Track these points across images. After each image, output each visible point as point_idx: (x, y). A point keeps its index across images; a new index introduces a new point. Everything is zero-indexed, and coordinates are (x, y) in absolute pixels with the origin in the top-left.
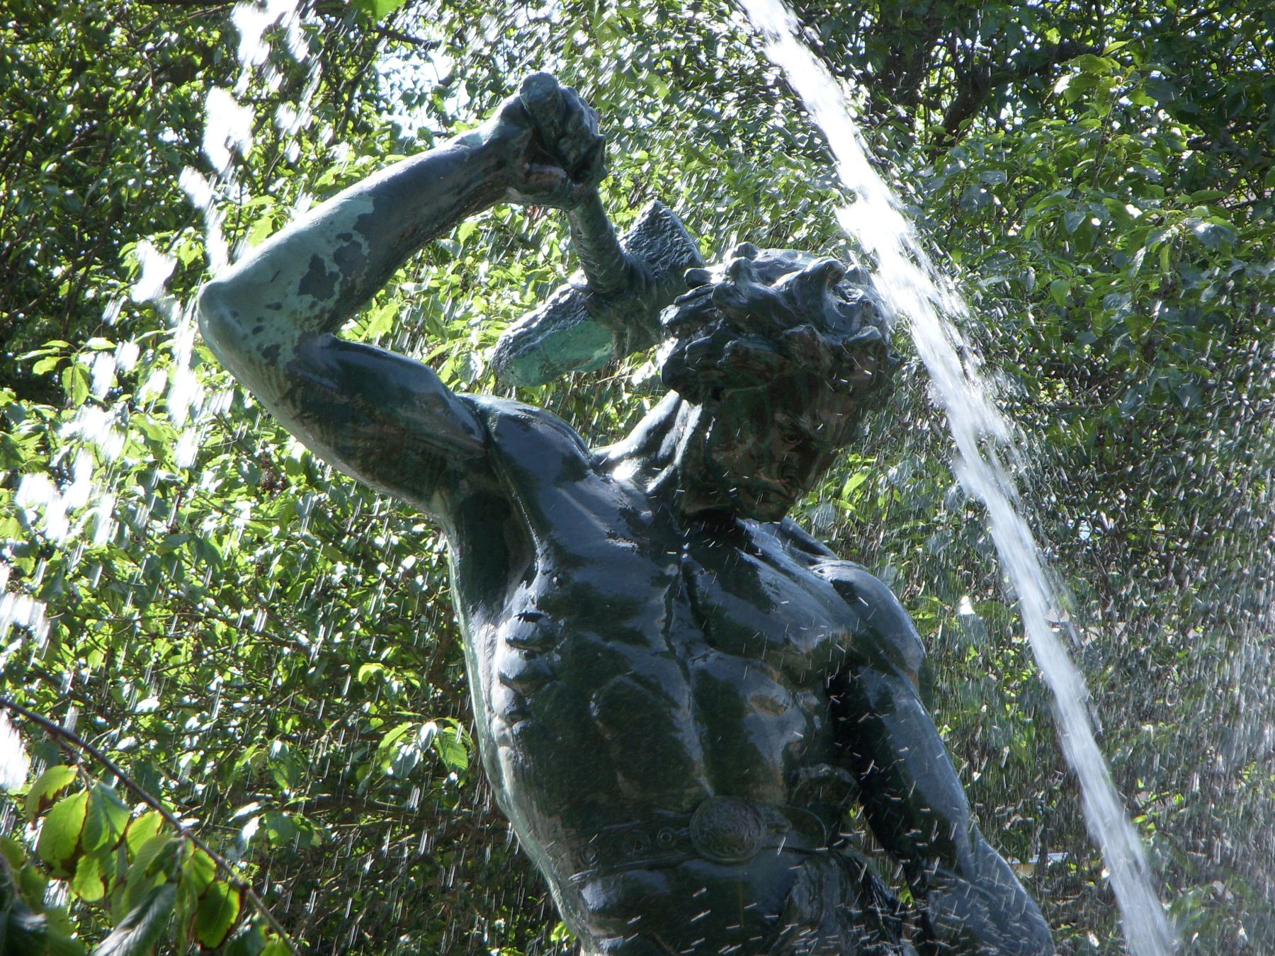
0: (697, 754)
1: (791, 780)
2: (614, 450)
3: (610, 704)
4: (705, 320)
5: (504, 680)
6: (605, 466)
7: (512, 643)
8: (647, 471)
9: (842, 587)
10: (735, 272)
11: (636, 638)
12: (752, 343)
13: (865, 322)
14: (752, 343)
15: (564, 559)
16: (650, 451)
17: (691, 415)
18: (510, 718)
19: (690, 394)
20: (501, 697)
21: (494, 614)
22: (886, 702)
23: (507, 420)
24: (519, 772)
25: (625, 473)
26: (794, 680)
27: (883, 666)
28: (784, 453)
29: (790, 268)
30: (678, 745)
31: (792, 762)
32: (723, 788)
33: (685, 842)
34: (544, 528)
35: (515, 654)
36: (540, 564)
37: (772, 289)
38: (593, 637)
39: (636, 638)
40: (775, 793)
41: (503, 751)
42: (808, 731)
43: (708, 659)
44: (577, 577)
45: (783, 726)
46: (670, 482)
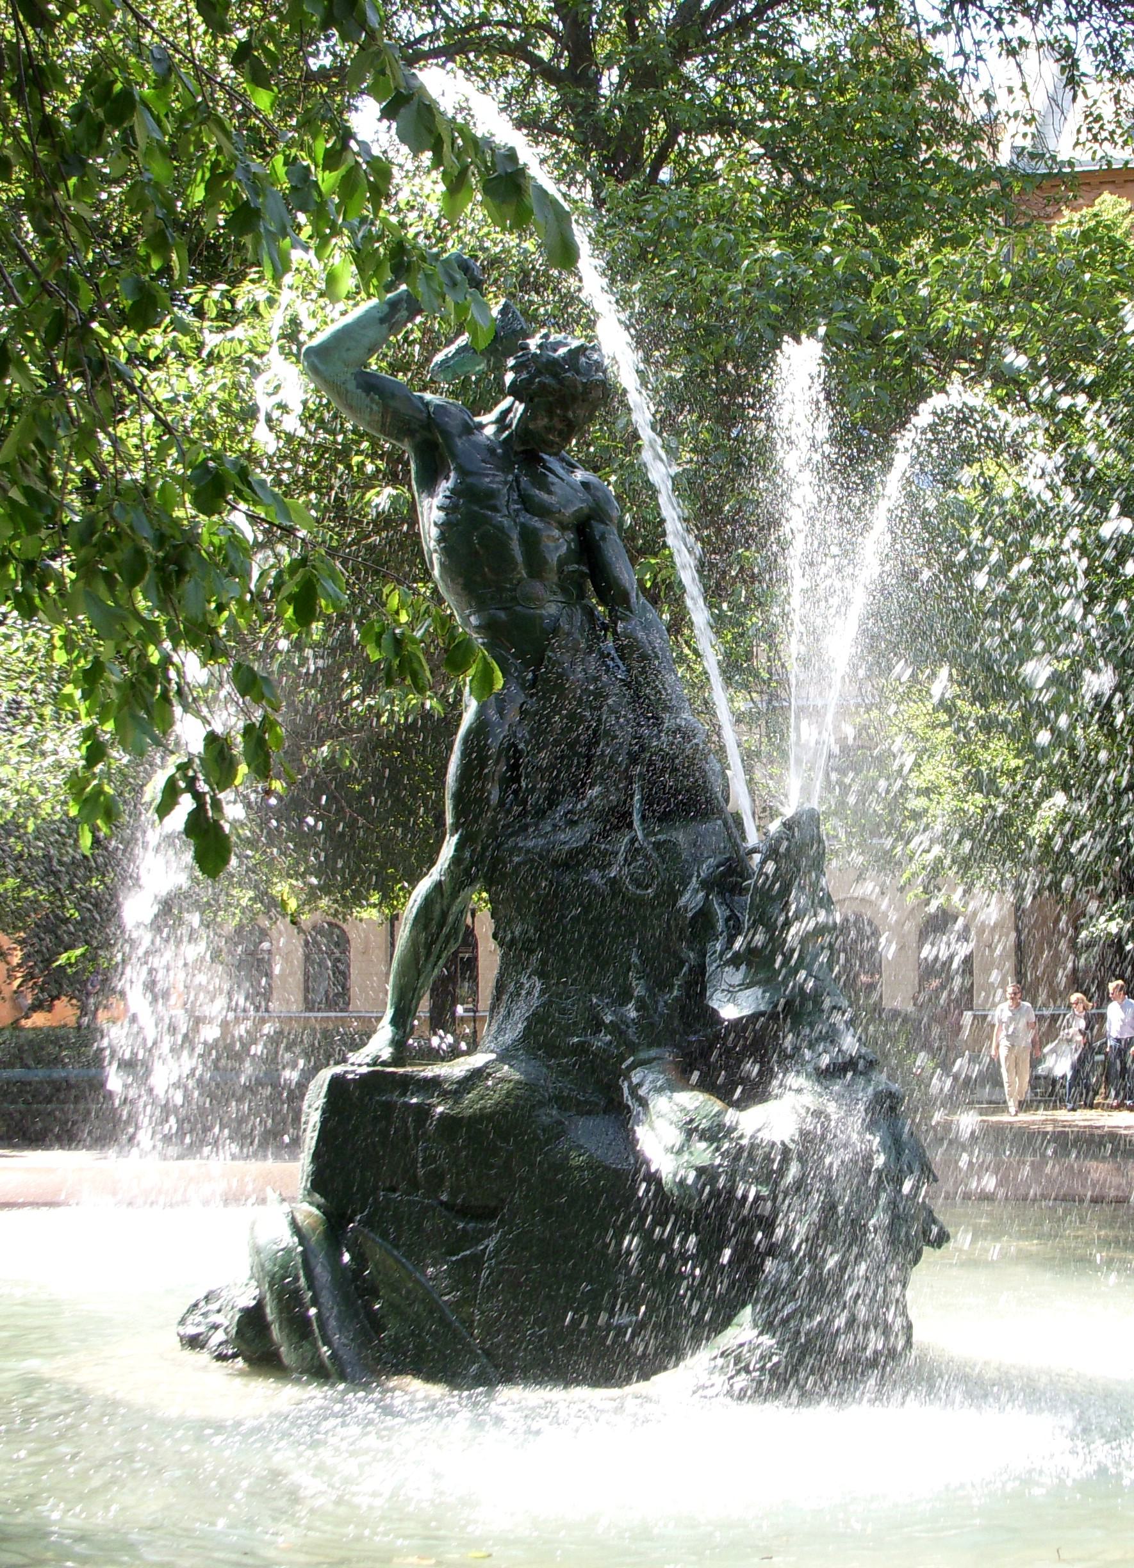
0: (519, 558)
1: (560, 571)
2: (484, 419)
3: (481, 538)
4: (527, 367)
5: (436, 524)
6: (481, 426)
7: (440, 508)
8: (500, 431)
9: (585, 485)
10: (540, 347)
11: (495, 509)
12: (548, 380)
13: (597, 371)
14: (548, 380)
15: (462, 472)
16: (501, 421)
17: (520, 408)
18: (439, 541)
19: (519, 397)
20: (434, 532)
21: (431, 494)
22: (603, 537)
23: (437, 406)
24: (442, 564)
25: (490, 431)
26: (563, 527)
27: (603, 522)
28: (560, 426)
29: (566, 345)
30: (513, 557)
31: (562, 562)
32: (531, 575)
33: (514, 599)
34: (454, 457)
35: (442, 514)
36: (452, 474)
37: (556, 355)
38: (476, 508)
39: (495, 509)
40: (554, 578)
41: (435, 556)
42: (569, 548)
43: (524, 518)
44: (469, 480)
45: (557, 548)
46: (511, 435)
